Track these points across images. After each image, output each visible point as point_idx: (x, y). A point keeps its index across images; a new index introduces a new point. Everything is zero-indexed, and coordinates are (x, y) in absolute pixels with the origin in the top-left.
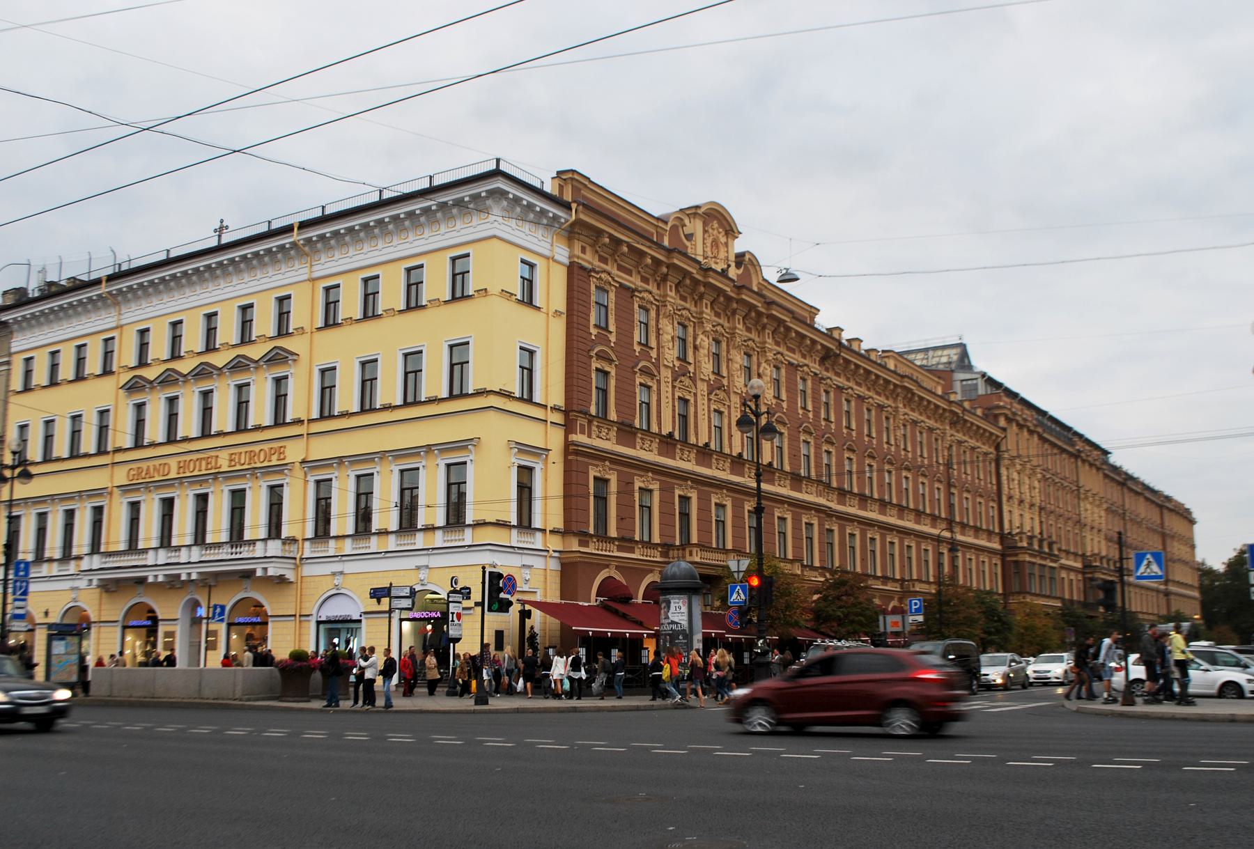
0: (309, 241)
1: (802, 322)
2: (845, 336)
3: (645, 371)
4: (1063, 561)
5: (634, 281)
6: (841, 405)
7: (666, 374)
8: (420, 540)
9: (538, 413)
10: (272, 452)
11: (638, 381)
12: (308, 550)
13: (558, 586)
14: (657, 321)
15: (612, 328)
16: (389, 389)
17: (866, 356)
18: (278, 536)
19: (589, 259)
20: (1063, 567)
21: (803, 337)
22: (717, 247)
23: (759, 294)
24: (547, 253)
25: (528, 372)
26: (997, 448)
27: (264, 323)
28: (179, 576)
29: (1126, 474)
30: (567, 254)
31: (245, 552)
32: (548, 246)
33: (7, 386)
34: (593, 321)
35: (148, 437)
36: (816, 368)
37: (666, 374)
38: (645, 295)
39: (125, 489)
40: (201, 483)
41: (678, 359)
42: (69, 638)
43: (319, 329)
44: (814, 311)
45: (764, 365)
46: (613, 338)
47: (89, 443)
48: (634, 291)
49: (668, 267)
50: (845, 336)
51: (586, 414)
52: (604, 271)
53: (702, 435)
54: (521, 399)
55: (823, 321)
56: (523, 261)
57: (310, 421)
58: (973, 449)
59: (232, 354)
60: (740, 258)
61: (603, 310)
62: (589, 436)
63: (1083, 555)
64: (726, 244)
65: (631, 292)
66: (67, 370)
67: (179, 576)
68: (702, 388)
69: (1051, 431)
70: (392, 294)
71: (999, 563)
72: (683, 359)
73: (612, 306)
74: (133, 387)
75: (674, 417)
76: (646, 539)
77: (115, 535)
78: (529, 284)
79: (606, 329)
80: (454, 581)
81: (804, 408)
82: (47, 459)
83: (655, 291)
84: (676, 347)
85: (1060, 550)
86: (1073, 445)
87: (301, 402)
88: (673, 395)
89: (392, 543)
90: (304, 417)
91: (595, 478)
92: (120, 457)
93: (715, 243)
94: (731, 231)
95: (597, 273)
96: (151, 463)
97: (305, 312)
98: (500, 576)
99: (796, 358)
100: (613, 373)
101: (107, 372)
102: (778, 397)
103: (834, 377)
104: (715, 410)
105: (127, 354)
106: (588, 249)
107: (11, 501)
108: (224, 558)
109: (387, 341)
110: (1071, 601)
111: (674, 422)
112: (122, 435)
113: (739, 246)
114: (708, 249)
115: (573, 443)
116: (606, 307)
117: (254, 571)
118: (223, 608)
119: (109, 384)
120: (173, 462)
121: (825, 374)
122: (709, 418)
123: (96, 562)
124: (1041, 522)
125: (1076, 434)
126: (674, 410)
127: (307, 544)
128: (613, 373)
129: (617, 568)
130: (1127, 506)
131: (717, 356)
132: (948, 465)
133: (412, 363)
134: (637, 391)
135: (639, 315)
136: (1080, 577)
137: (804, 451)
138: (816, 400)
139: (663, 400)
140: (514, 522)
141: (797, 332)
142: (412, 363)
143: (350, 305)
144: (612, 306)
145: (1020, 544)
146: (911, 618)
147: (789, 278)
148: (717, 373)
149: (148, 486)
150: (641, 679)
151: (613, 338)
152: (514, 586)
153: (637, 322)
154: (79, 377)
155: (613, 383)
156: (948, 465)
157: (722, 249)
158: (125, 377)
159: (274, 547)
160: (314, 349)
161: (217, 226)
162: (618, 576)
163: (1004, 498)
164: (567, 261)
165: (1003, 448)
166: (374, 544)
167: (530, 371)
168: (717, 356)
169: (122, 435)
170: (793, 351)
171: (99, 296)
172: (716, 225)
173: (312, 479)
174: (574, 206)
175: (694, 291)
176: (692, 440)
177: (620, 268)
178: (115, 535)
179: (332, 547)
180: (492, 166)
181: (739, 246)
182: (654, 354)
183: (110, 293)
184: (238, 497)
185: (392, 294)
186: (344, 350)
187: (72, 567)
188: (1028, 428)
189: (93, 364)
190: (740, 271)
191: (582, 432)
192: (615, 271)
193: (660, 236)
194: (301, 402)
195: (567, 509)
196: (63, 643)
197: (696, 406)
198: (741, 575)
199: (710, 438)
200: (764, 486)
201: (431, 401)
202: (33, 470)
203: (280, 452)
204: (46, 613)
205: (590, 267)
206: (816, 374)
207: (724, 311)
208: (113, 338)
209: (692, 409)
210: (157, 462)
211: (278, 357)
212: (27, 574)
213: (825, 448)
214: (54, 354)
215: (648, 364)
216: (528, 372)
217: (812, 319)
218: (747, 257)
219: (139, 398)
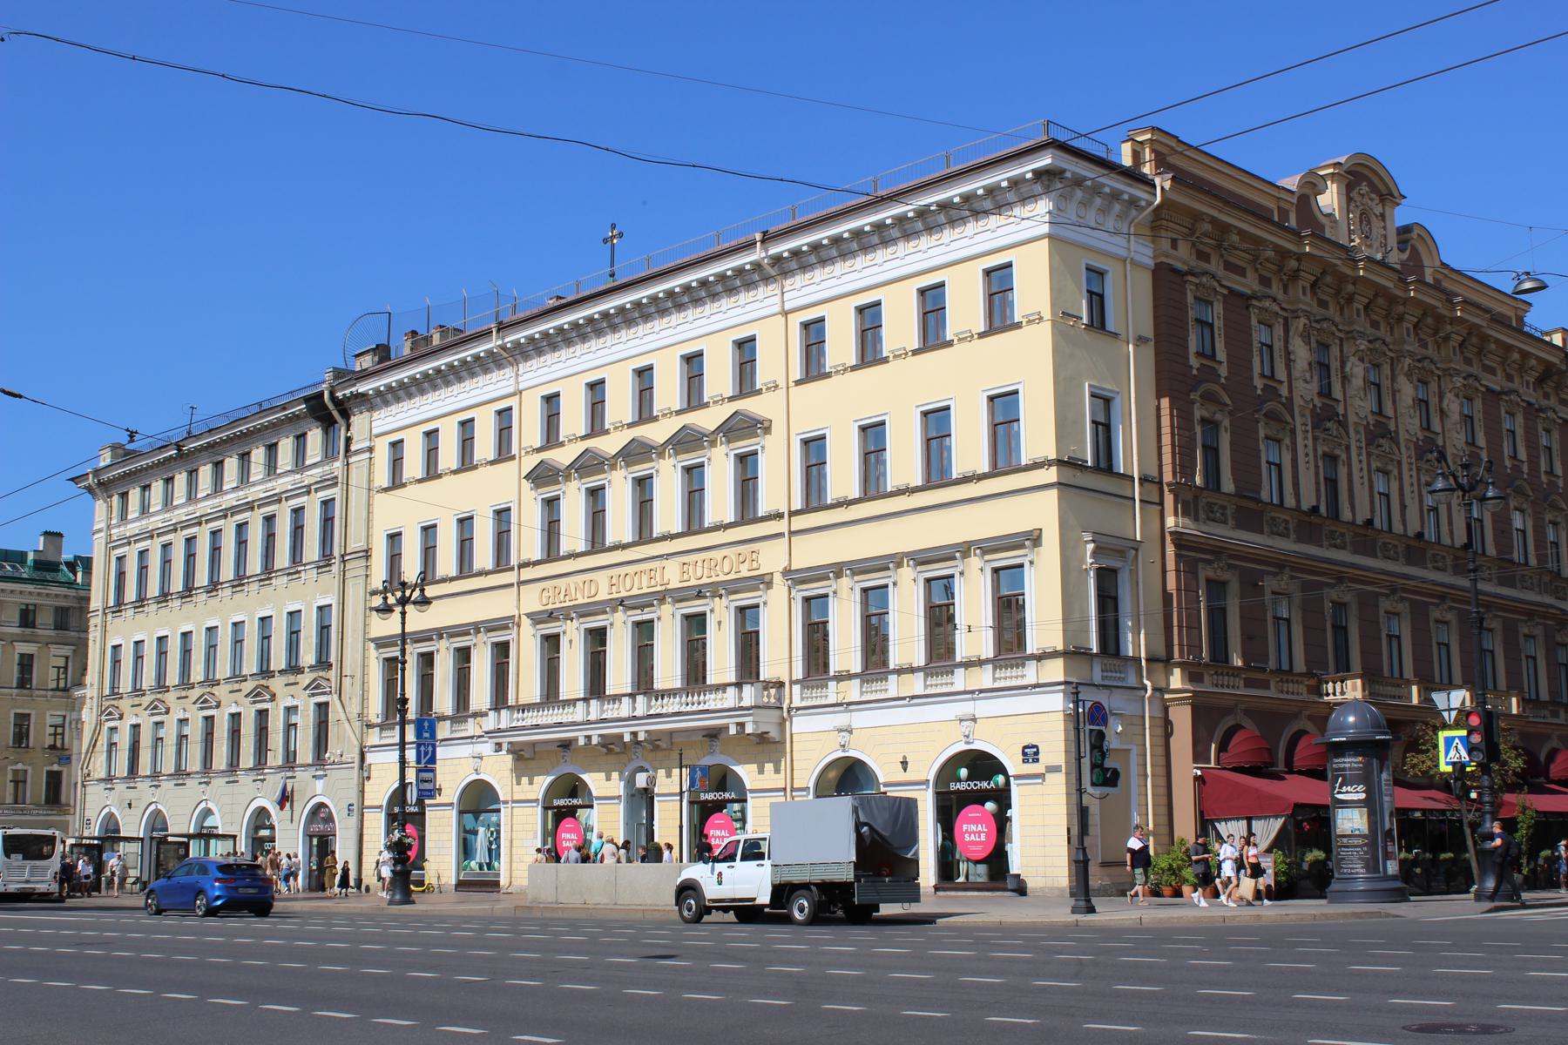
0: (777, 260)
1: (1500, 321)
3: (1272, 416)
5: (1248, 284)
7: (1301, 422)
8: (960, 680)
11: (1262, 434)
12: (796, 696)
14: (1286, 341)
15: (1221, 355)
16: (904, 460)
19: (1183, 256)
21: (1509, 348)
22: (1369, 223)
24: (1123, 253)
25: (1104, 430)
27: (719, 376)
28: (621, 736)
30: (1149, 252)
31: (713, 701)
32: (1125, 244)
33: (370, 481)
35: (565, 546)
36: (1531, 395)
37: (1301, 422)
38: (1267, 303)
39: (537, 618)
40: (642, 607)
41: (1320, 394)
43: (798, 383)
45: (1449, 396)
46: (1223, 371)
47: (483, 555)
48: (1250, 298)
49: (1298, 260)
52: (1205, 273)
53: (1358, 507)
54: (1097, 469)
57: (792, 514)
60: (1405, 231)
64: (1383, 216)
65: (1245, 300)
66: (448, 456)
67: (621, 736)
68: (1355, 439)
70: (901, 326)
72: (1325, 392)
73: (1218, 324)
74: (542, 476)
75: (1317, 483)
76: (1285, 667)
77: (527, 682)
79: (1213, 357)
81: (1514, 457)
83: (1280, 296)
84: (1316, 378)
87: (778, 483)
88: (1315, 450)
89: (916, 684)
90: (784, 509)
91: (1208, 581)
92: (527, 574)
94: (1388, 195)
97: (778, 356)
99: (1495, 382)
102: (1472, 443)
103: (1558, 408)
104: (1378, 470)
105: (529, 430)
107: (403, 636)
108: (678, 712)
109: (899, 392)
111: (1318, 490)
112: (528, 541)
113: (1401, 216)
116: (1211, 326)
119: (509, 468)
121: (1544, 403)
122: (1317, 467)
123: (505, 719)
126: (1317, 473)
127: (796, 688)
131: (1324, 368)
133: (936, 422)
134: (1262, 447)
135: (1260, 335)
138: (1532, 444)
139: (1407, 489)
141: (1498, 341)
142: (936, 422)
143: (841, 344)
144: (1218, 324)
148: (1325, 392)
149: (565, 614)
150: (558, 859)
151: (1223, 371)
153: (1256, 345)
154: (467, 463)
157: (1377, 224)
158: (530, 462)
159: (749, 695)
160: (792, 410)
164: (1151, 263)
166: (893, 686)
169: (528, 541)
170: (1492, 371)
171: (490, 353)
173: (798, 597)
175: (1338, 292)
176: (1346, 515)
177: (1229, 266)
178: (527, 682)
179: (833, 692)
181: (1401, 216)
182: (1284, 391)
183: (503, 348)
184: (695, 625)
186: (835, 409)
187: (471, 727)
189: (485, 445)
190: (1405, 256)
193: (1284, 213)
194: (778, 483)
198: (1454, 714)
199: (1372, 511)
201: (966, 480)
205: (1185, 268)
206: (1530, 404)
207: (1502, 364)
208: (510, 409)
210: (579, 578)
211: (740, 427)
212: (433, 735)
213: (1549, 517)
216: (1104, 430)
217: (1520, 320)
218: (1416, 231)
219: (549, 492)
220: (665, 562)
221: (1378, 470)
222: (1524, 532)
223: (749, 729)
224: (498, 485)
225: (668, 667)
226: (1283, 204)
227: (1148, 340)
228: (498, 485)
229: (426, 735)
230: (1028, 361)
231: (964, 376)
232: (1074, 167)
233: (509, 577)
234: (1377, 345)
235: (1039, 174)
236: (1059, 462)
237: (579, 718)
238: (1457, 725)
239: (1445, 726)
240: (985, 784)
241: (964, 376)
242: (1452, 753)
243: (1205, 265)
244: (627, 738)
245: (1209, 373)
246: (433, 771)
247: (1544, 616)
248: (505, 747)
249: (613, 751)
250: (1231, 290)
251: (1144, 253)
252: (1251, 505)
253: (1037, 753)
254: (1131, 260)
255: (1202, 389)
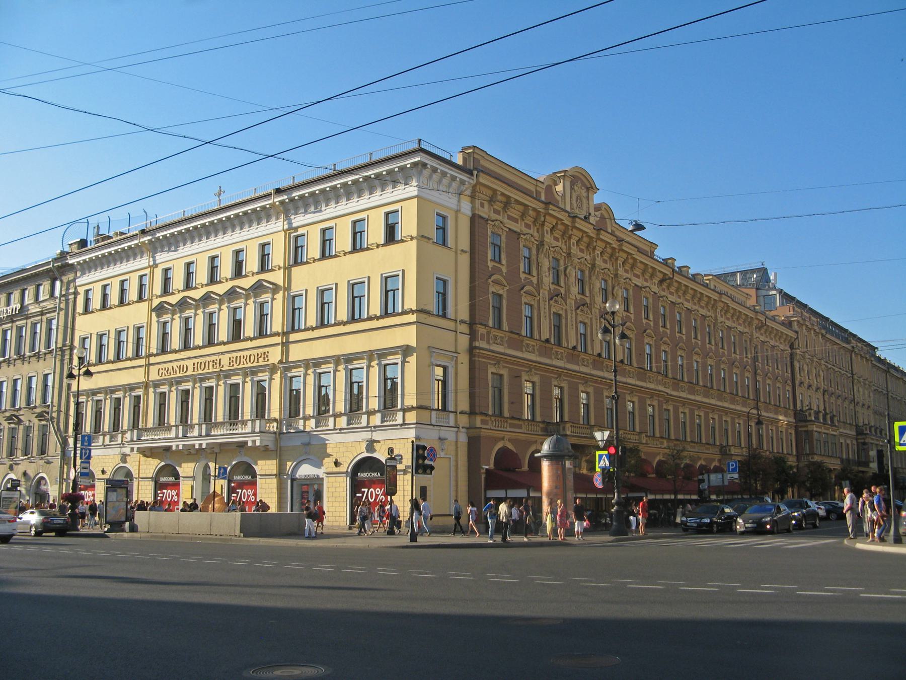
2: (678, 264)
4: (841, 430)
6: (675, 316)
9: (451, 325)
10: (258, 357)
13: (466, 468)
17: (694, 278)
18: (263, 416)
20: (842, 435)
22: (581, 201)
23: (613, 234)
25: (443, 296)
26: (792, 347)
29: (889, 364)
34: (489, 257)
36: (655, 289)
42: (119, 490)
44: (654, 246)
46: (504, 269)
50: (678, 264)
51: (485, 326)
55: (661, 253)
56: (438, 214)
58: (773, 347)
59: (230, 285)
60: (598, 208)
61: (497, 249)
62: (488, 343)
63: (857, 426)
64: (588, 198)
66: (114, 299)
69: (832, 333)
71: (793, 432)
73: (503, 245)
75: (550, 327)
78: (443, 229)
79: (500, 262)
80: (391, 451)
82: (100, 362)
85: (839, 421)
86: (848, 342)
90: (280, 331)
92: (153, 360)
93: (579, 198)
94: (591, 188)
95: (493, 221)
96: (175, 364)
98: (424, 448)
100: (505, 296)
101: (140, 299)
104: (581, 322)
106: (486, 204)
108: (221, 435)
110: (848, 460)
111: (550, 331)
113: (597, 199)
114: (574, 202)
115: (476, 348)
116: (500, 247)
117: (246, 442)
118: (225, 469)
119: (144, 306)
120: (190, 363)
122: (550, 319)
124: (824, 401)
125: (851, 334)
128: (505, 296)
129: (510, 440)
130: (890, 388)
131: (582, 281)
132: (755, 359)
136: (855, 442)
137: (648, 351)
138: (656, 313)
140: (435, 312)
145: (809, 418)
146: (729, 476)
147: (639, 227)
152: (435, 455)
154: (122, 302)
155: (505, 302)
156: (755, 359)
158: (156, 302)
161: (217, 191)
162: (510, 446)
163: (797, 383)
165: (796, 346)
167: (444, 295)
168: (582, 281)
170: (638, 277)
172: (580, 185)
174: (475, 173)
177: (509, 218)
180: (416, 146)
181: (597, 199)
184: (234, 390)
185: (343, 240)
188: (815, 330)
189: (132, 294)
191: (483, 339)
192: (506, 220)
195: (472, 396)
196: (115, 493)
197: (566, 319)
200: (618, 378)
202: (92, 369)
203: (266, 356)
204: (103, 472)
209: (563, 321)
214: (105, 287)
215: (532, 288)
216: (443, 296)
217: (652, 253)
220: (221, 357)
221: (581, 322)
222: (650, 355)
223: (258, 444)
224: (137, 314)
225: (220, 412)
226: (538, 189)
227: (466, 252)
228: (137, 314)
229: (86, 444)
230: (404, 258)
231: (374, 265)
232: (431, 162)
233: (142, 362)
234: (583, 260)
235: (415, 165)
236: (417, 311)
237: (172, 438)
238: (603, 449)
239: (599, 449)
240: (850, 530)
241: (374, 265)
242: (602, 462)
243: (528, 231)
244: (197, 447)
245: (497, 271)
246: (89, 463)
247: (659, 396)
248: (135, 449)
249: (191, 454)
250: (510, 229)
251: (466, 207)
252: (516, 336)
253: (401, 459)
254: (459, 208)
255: (493, 278)
